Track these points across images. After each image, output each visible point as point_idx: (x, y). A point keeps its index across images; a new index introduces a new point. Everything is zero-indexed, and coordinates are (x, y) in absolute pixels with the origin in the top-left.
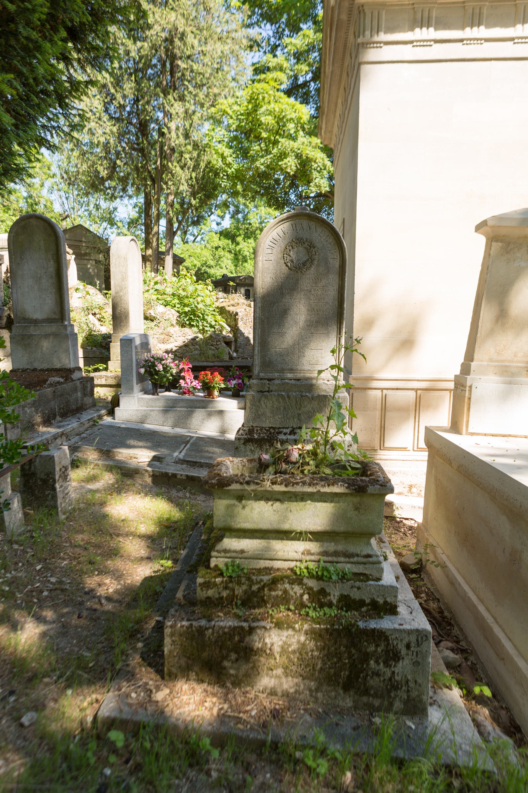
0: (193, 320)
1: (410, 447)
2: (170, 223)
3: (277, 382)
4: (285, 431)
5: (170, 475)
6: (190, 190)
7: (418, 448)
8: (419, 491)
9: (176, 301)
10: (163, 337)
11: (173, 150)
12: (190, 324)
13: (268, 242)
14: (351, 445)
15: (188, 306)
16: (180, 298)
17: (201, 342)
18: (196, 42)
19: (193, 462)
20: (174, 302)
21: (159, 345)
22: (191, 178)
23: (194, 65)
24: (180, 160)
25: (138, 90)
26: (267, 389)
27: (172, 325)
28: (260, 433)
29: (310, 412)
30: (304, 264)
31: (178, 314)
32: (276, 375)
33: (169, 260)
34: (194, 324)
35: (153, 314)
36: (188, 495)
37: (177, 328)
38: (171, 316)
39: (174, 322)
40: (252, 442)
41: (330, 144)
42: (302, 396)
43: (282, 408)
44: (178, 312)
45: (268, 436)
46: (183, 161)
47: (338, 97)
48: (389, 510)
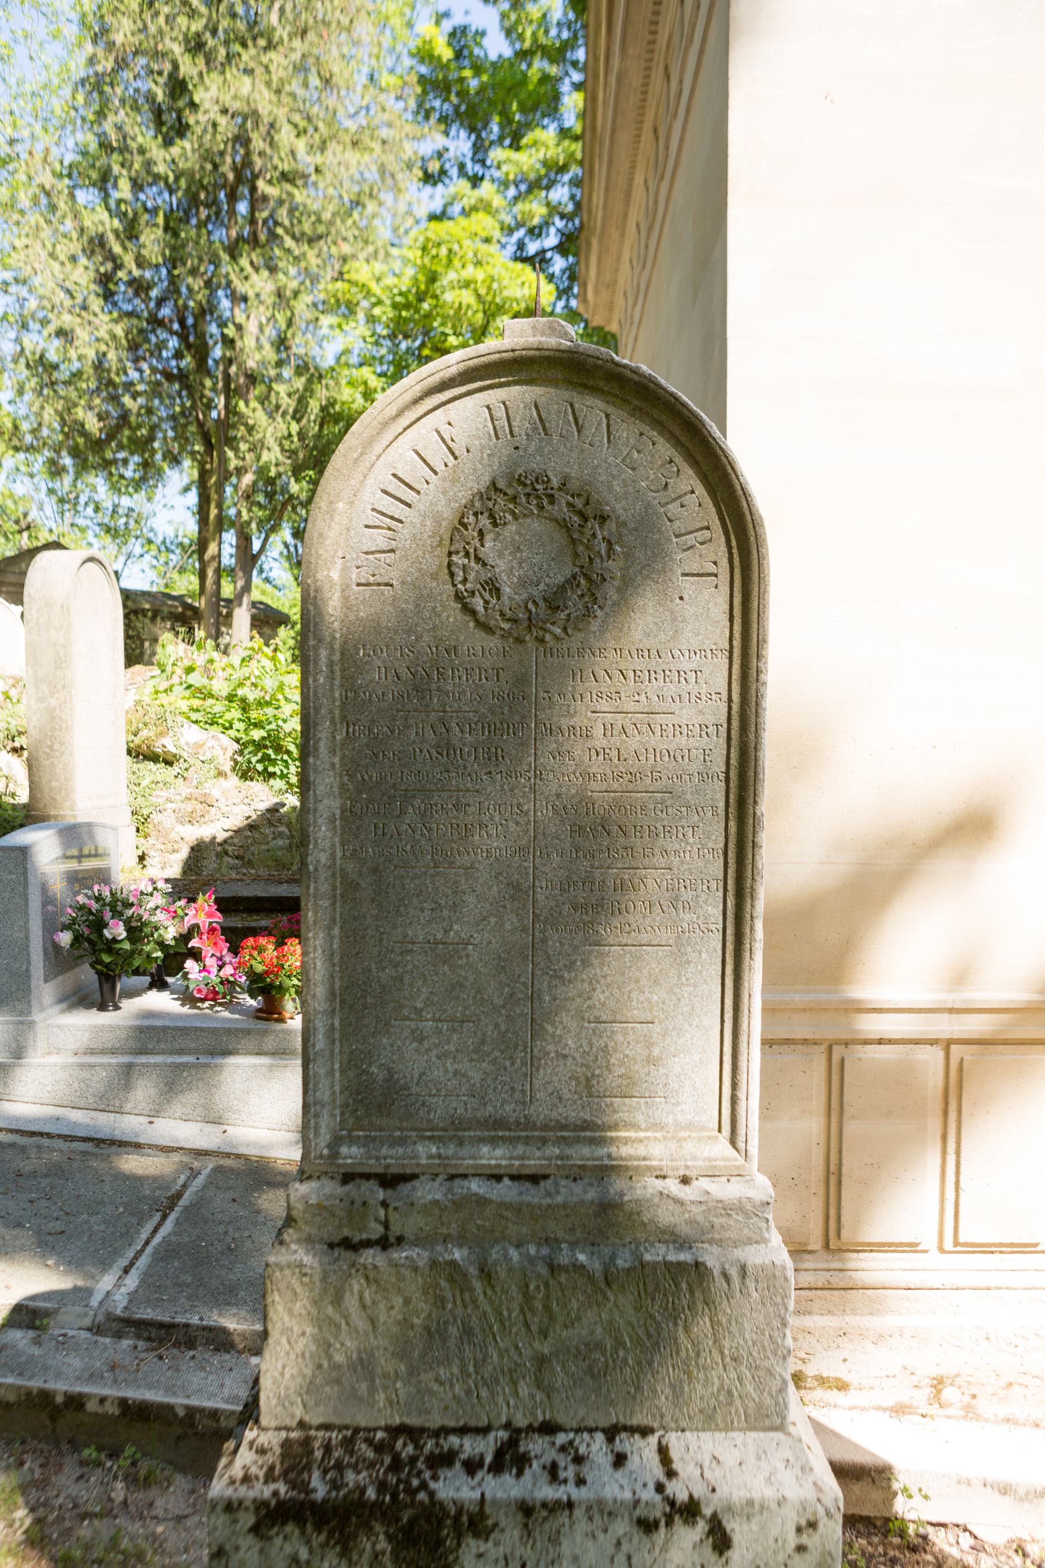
0: (274, 762)
1: (929, 1241)
2: (245, 540)
3: (427, 1191)
4: (470, 1446)
5: (59, 1399)
6: (289, 462)
7: (956, 1243)
8: (967, 1399)
9: (235, 714)
10: (189, 807)
11: (252, 378)
12: (266, 769)
13: (371, 496)
14: (812, 1525)
15: (258, 725)
16: (245, 706)
17: (294, 816)
18: (301, 145)
19: (162, 1325)
20: (228, 716)
21: (179, 828)
22: (290, 435)
23: (296, 192)
24: (267, 397)
25: (173, 248)
26: (376, 1231)
27: (221, 774)
28: (339, 1467)
29: (599, 1346)
30: (554, 602)
31: (236, 747)
32: (424, 1152)
33: (242, 617)
34: (276, 770)
35: (172, 749)
36: (119, 1491)
37: (234, 780)
38: (217, 752)
39: (227, 766)
40: (301, 1523)
41: (609, 321)
42: (553, 1268)
43: (453, 1330)
44: (237, 741)
45: (382, 1487)
46: (273, 400)
47: (633, 166)
48: (876, 1495)
